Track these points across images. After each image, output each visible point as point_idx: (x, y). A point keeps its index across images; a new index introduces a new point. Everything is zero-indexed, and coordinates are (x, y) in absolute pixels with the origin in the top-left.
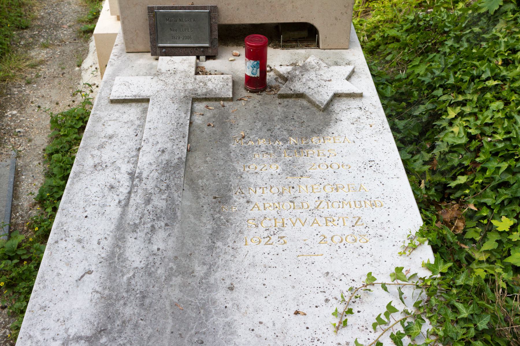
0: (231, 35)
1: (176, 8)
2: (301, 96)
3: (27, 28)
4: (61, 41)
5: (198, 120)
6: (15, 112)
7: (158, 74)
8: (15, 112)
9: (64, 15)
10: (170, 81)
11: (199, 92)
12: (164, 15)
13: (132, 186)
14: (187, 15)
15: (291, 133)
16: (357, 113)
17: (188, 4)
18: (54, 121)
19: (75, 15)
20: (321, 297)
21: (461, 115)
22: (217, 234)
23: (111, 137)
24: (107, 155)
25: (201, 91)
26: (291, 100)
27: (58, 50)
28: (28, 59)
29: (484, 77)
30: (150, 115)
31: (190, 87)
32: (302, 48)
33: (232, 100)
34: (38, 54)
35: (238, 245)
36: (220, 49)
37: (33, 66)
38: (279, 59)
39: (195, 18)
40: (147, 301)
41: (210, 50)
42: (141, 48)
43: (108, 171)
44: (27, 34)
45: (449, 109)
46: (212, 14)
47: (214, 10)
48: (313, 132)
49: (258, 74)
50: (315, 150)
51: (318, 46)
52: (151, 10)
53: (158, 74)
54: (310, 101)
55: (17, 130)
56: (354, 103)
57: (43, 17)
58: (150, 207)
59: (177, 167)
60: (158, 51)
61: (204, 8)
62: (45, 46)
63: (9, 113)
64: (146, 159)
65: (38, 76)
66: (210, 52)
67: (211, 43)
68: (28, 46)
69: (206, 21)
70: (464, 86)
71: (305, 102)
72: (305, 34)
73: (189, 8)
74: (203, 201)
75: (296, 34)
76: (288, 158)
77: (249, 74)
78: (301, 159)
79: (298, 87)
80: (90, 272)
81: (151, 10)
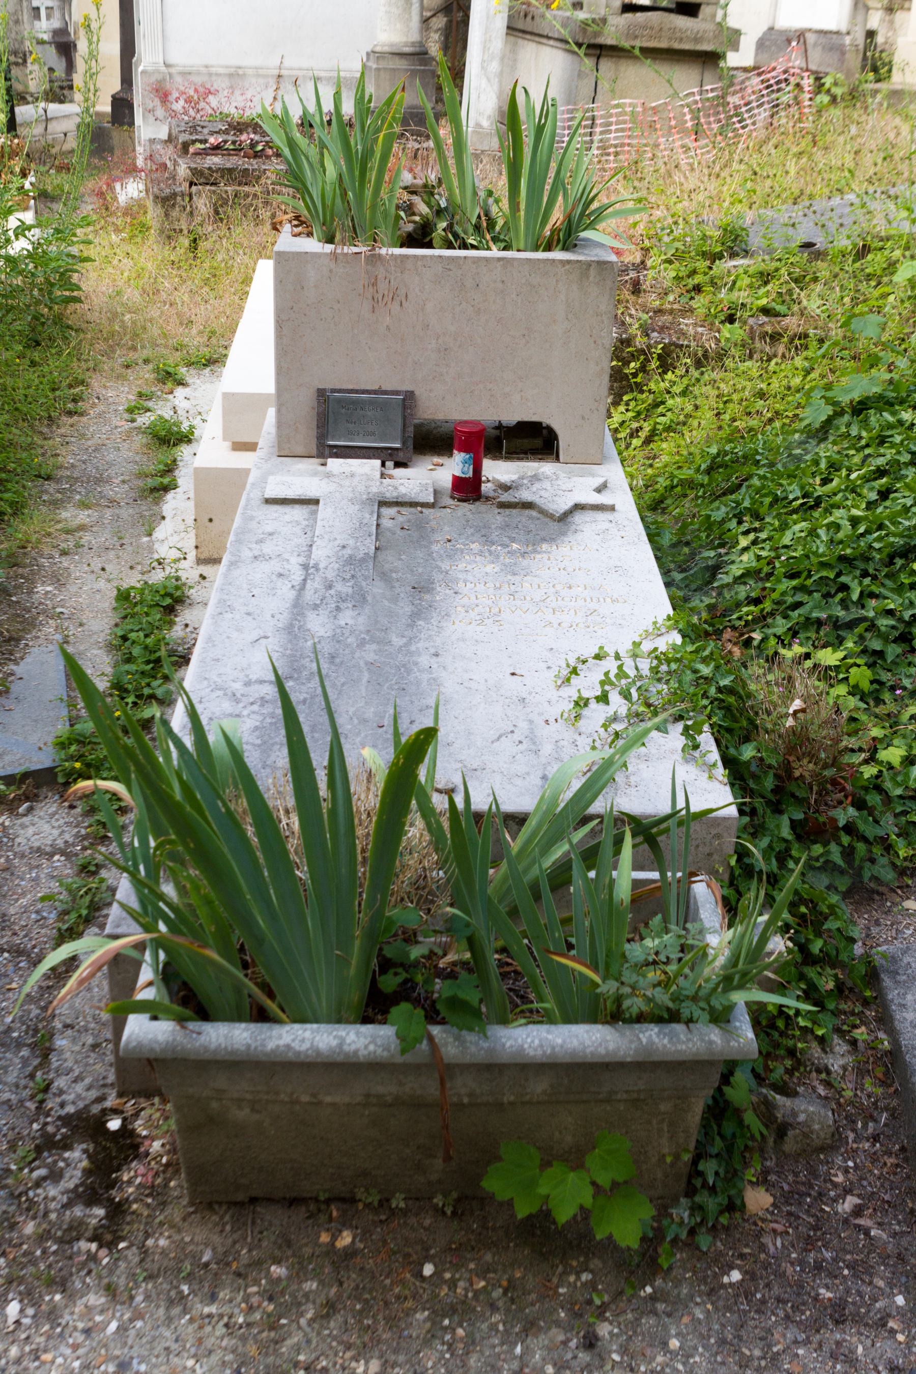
0: (430, 441)
1: (357, 392)
2: (528, 505)
3: (48, 478)
4: (112, 501)
5: (386, 523)
6: (49, 588)
7: (329, 475)
8: (49, 588)
9: (111, 464)
10: (347, 483)
11: (388, 495)
12: (339, 401)
13: (307, 575)
14: (371, 402)
15: (513, 540)
16: (606, 525)
17: (376, 387)
18: (123, 596)
19: (130, 466)
20: (544, 665)
21: (755, 542)
22: (416, 615)
23: (271, 534)
24: (268, 548)
25: (390, 495)
26: (514, 511)
27: (108, 513)
28: (59, 522)
29: (791, 497)
30: (320, 515)
31: (374, 490)
32: (534, 460)
33: (432, 506)
34: (71, 515)
35: (443, 624)
36: (415, 458)
37: (68, 532)
38: (497, 471)
39: (384, 406)
40: (338, 660)
41: (401, 454)
42: (300, 450)
43: (273, 562)
44: (51, 487)
45: (741, 538)
46: (407, 403)
47: (409, 399)
48: (544, 540)
49: (470, 474)
50: (545, 556)
51: (557, 459)
52: (321, 393)
53: (329, 475)
54: (543, 512)
55: (59, 610)
56: (601, 516)
57: (73, 466)
58: (332, 592)
59: (363, 560)
60: (327, 451)
61: (397, 393)
62: (84, 505)
63: (40, 589)
64: (322, 553)
65: (78, 546)
66: (401, 456)
67: (404, 443)
68: (55, 504)
69: (399, 411)
70: (763, 511)
71: (534, 513)
72: (538, 443)
73: (375, 392)
74: (398, 590)
75: (526, 443)
76: (507, 560)
77: (458, 473)
78: (525, 562)
79: (525, 495)
80: (266, 637)
81: (321, 393)
